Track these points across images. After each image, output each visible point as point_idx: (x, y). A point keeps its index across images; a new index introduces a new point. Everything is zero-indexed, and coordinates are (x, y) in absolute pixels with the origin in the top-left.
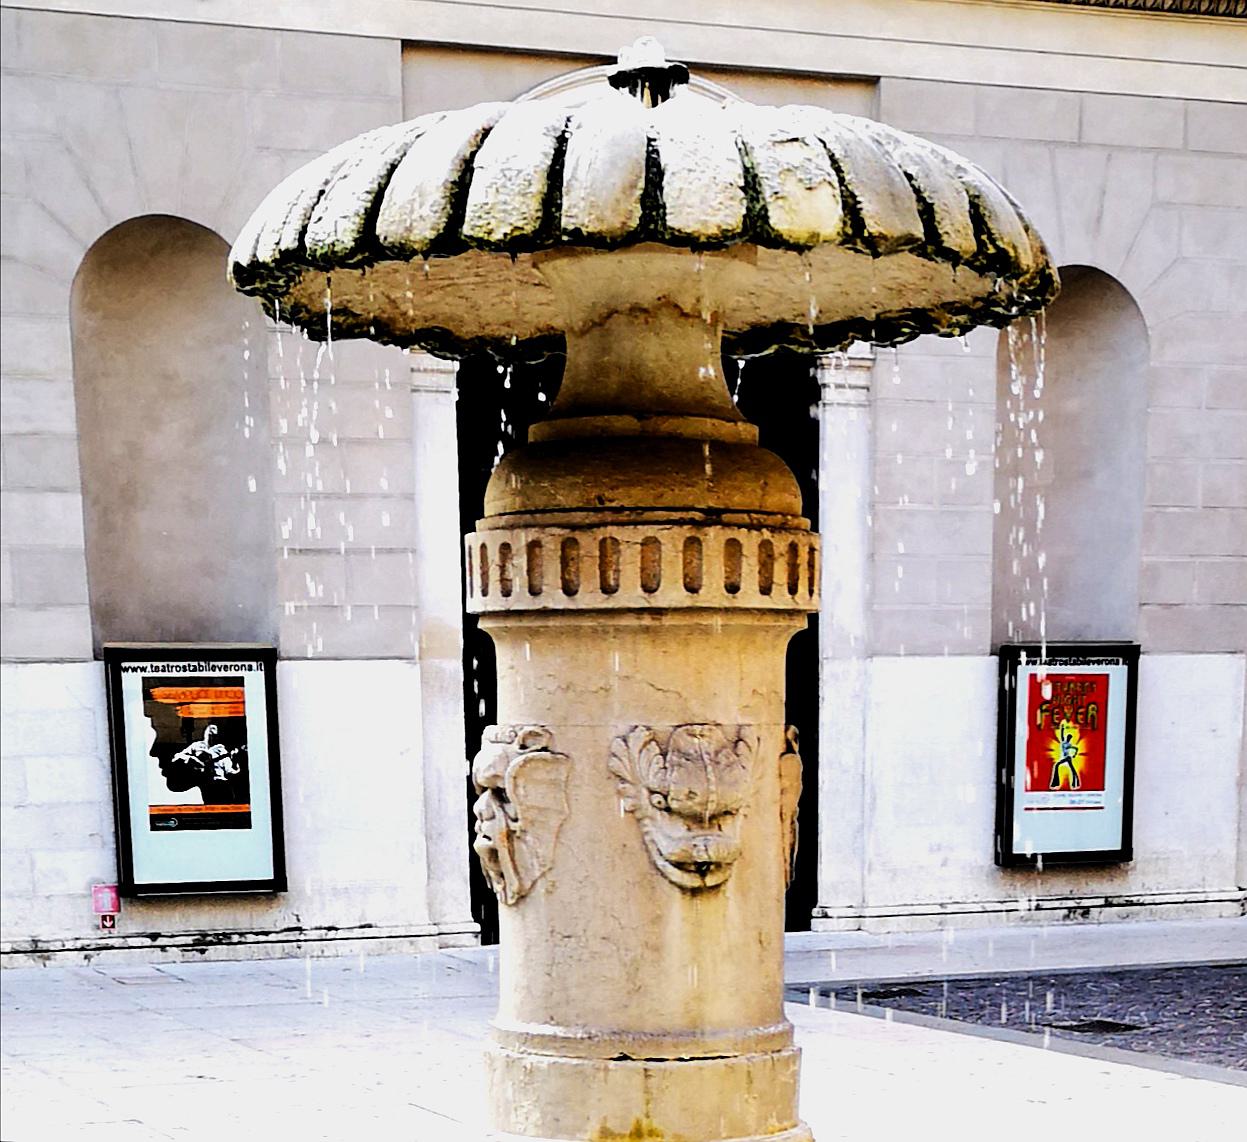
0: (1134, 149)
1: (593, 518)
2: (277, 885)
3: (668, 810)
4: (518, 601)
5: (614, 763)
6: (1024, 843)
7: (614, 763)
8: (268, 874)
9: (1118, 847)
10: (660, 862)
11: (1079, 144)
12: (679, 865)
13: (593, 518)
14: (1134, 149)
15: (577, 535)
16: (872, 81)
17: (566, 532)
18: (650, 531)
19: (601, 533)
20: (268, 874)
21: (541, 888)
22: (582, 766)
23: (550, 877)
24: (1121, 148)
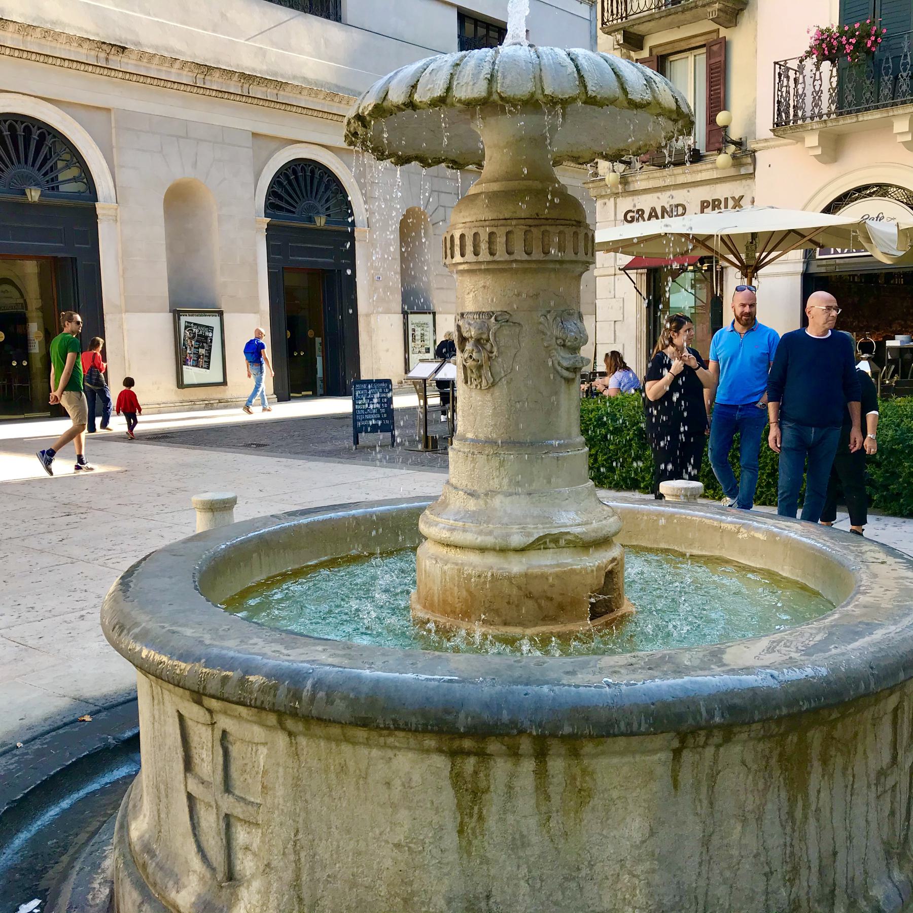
0: (205, 141)
1: (536, 222)
2: (224, 383)
3: (564, 346)
4: (500, 256)
5: (541, 327)
6: (187, 380)
7: (541, 327)
8: (221, 380)
9: (362, 378)
10: (559, 368)
11: (187, 137)
12: (567, 369)
13: (536, 222)
14: (205, 141)
15: (532, 229)
16: (108, 110)
17: (528, 228)
18: (561, 228)
19: (543, 228)
20: (221, 380)
21: (504, 381)
22: (526, 327)
23: (508, 376)
24: (202, 140)
